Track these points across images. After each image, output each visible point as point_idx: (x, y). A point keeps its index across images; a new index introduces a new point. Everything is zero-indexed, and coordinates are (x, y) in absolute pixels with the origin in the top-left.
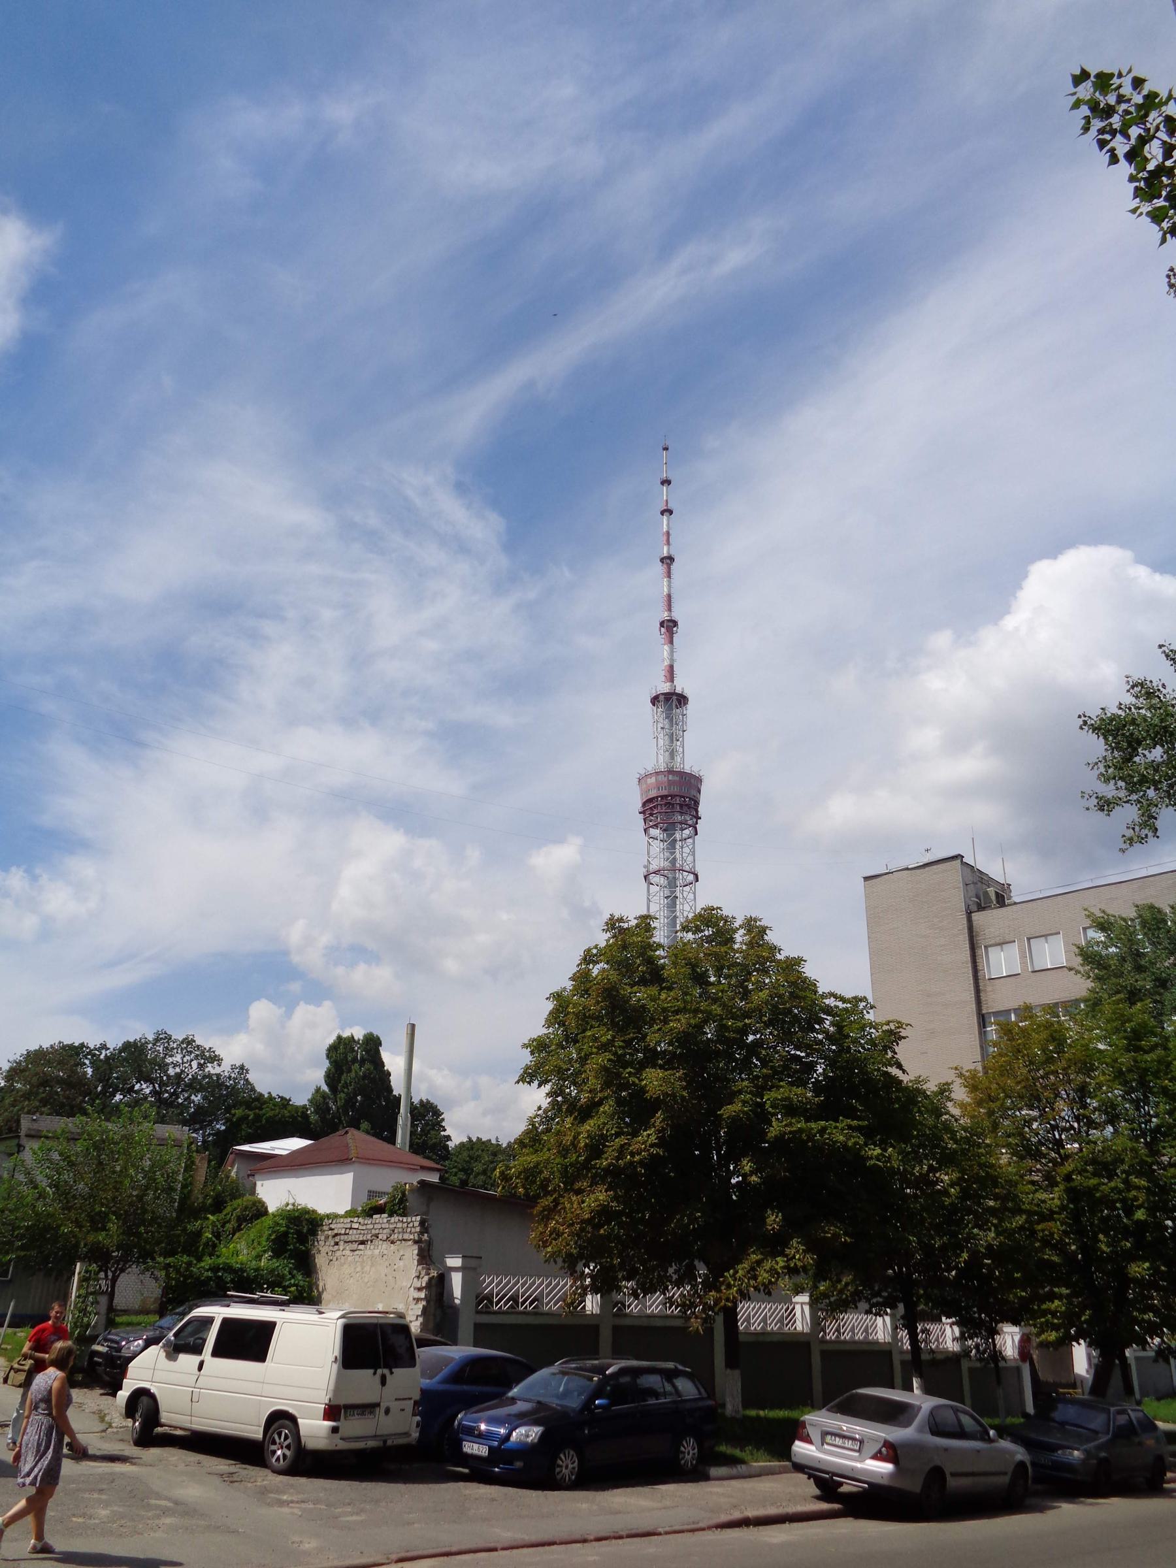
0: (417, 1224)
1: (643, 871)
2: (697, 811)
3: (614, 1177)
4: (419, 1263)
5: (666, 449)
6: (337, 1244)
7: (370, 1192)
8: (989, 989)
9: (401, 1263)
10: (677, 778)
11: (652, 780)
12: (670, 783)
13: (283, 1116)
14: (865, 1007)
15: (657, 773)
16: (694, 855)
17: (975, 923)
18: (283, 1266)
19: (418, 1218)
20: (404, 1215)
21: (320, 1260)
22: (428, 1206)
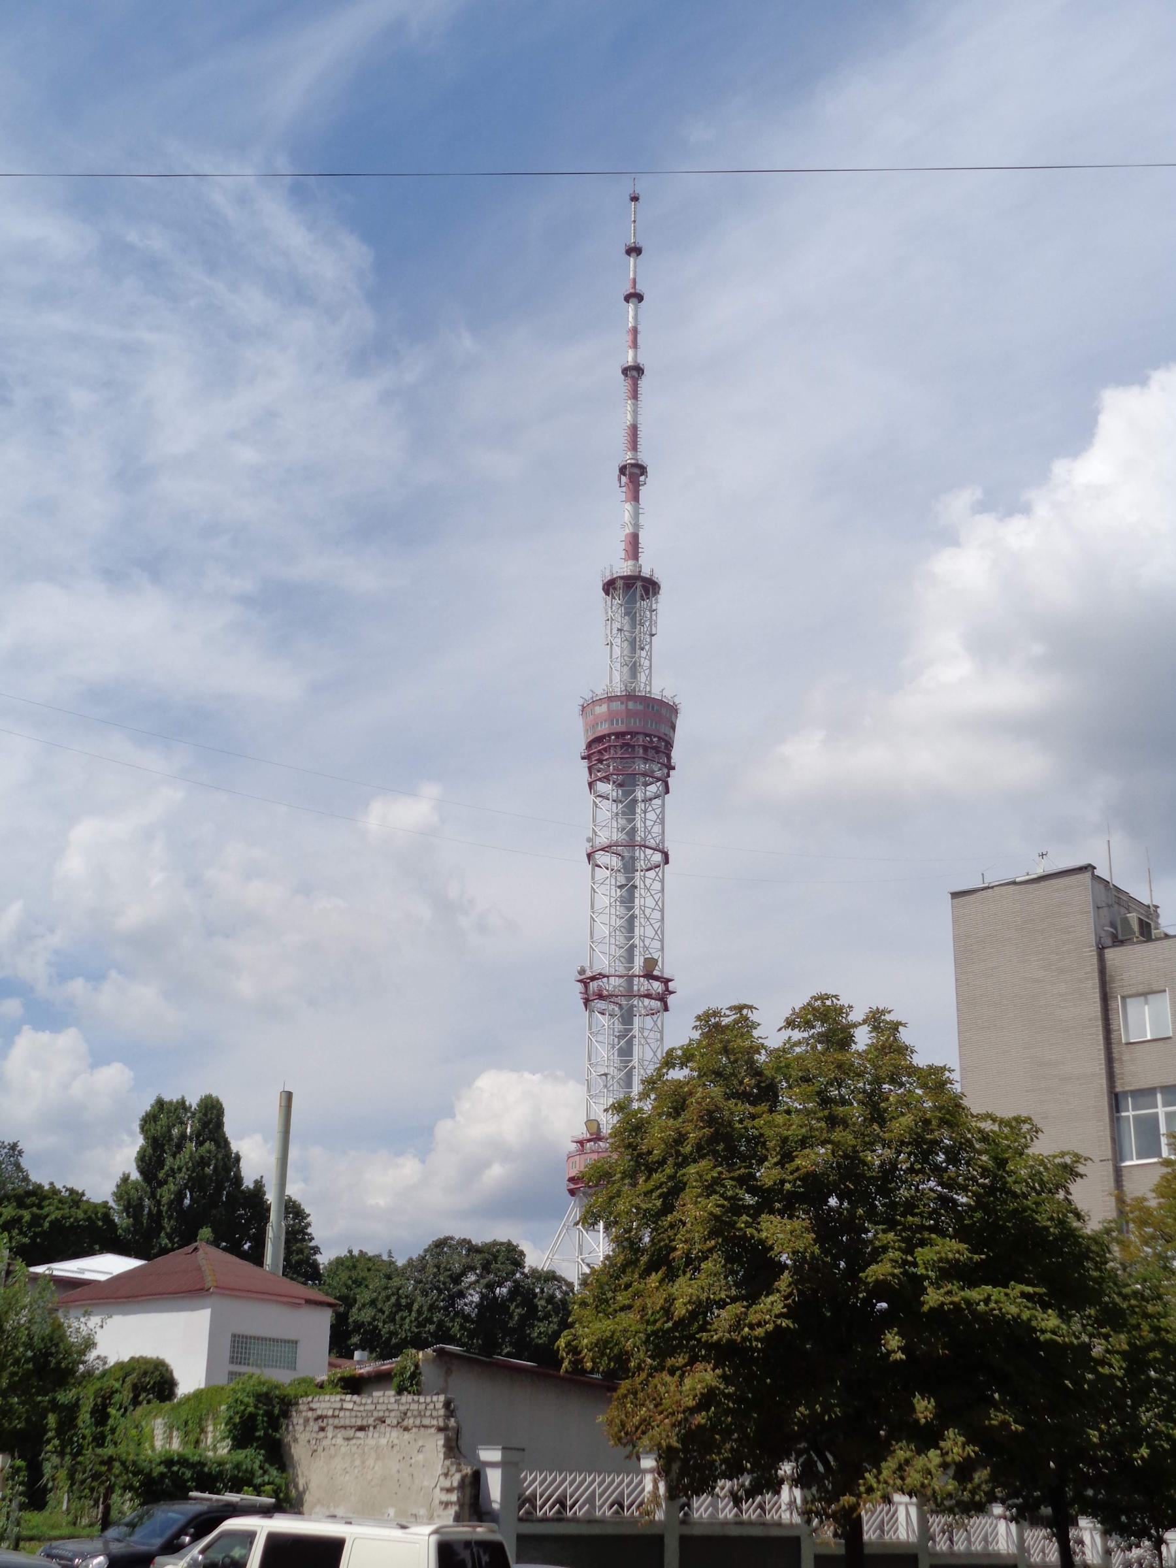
0: (440, 1405)
1: (587, 847)
2: (669, 758)
3: (723, 1353)
4: (447, 1457)
5: (635, 199)
6: (322, 1429)
7: (234, 1336)
8: (1126, 1057)
9: (421, 1457)
10: (640, 707)
11: (602, 709)
12: (630, 714)
13: (76, 1220)
14: (1029, 1131)
15: (610, 699)
16: (663, 823)
17: (1109, 963)
18: (251, 1458)
19: (442, 1398)
20: (419, 1393)
21: (299, 1451)
22: (446, 1381)
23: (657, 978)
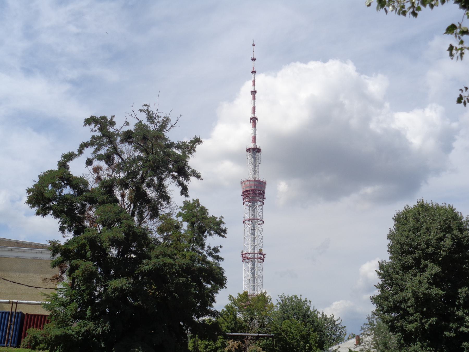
1: (243, 219)
2: (264, 196)
11: (248, 183)
12: (255, 185)
23: (262, 254)
